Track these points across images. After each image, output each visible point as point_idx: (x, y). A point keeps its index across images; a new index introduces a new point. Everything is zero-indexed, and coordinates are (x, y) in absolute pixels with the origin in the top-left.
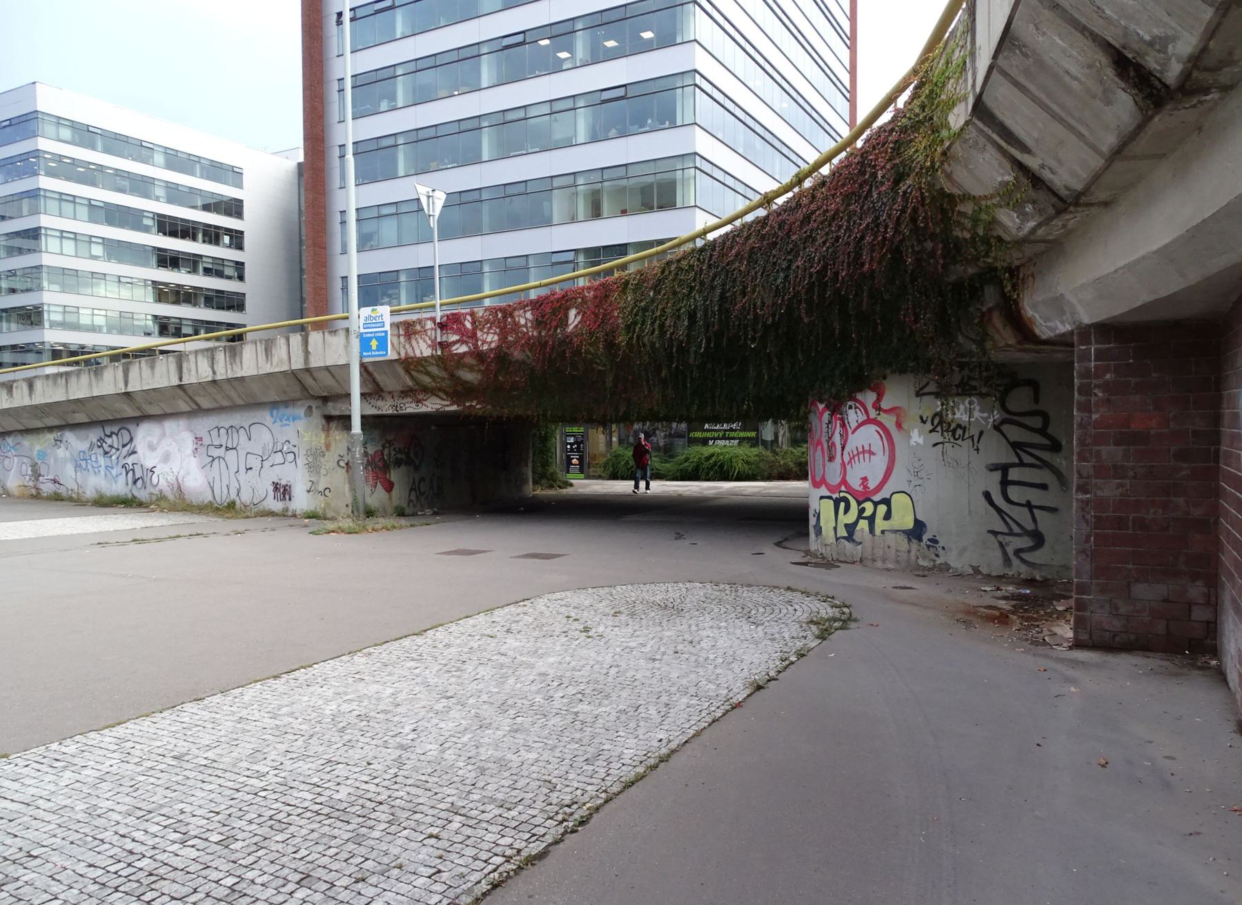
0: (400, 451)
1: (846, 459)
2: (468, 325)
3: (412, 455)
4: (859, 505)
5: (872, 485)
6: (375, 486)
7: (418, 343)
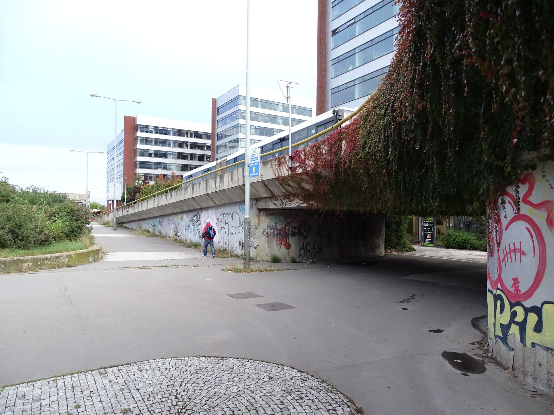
0: (295, 228)
1: (502, 257)
2: (303, 157)
3: (302, 230)
4: (511, 307)
5: (524, 288)
6: (281, 246)
7: (283, 168)
